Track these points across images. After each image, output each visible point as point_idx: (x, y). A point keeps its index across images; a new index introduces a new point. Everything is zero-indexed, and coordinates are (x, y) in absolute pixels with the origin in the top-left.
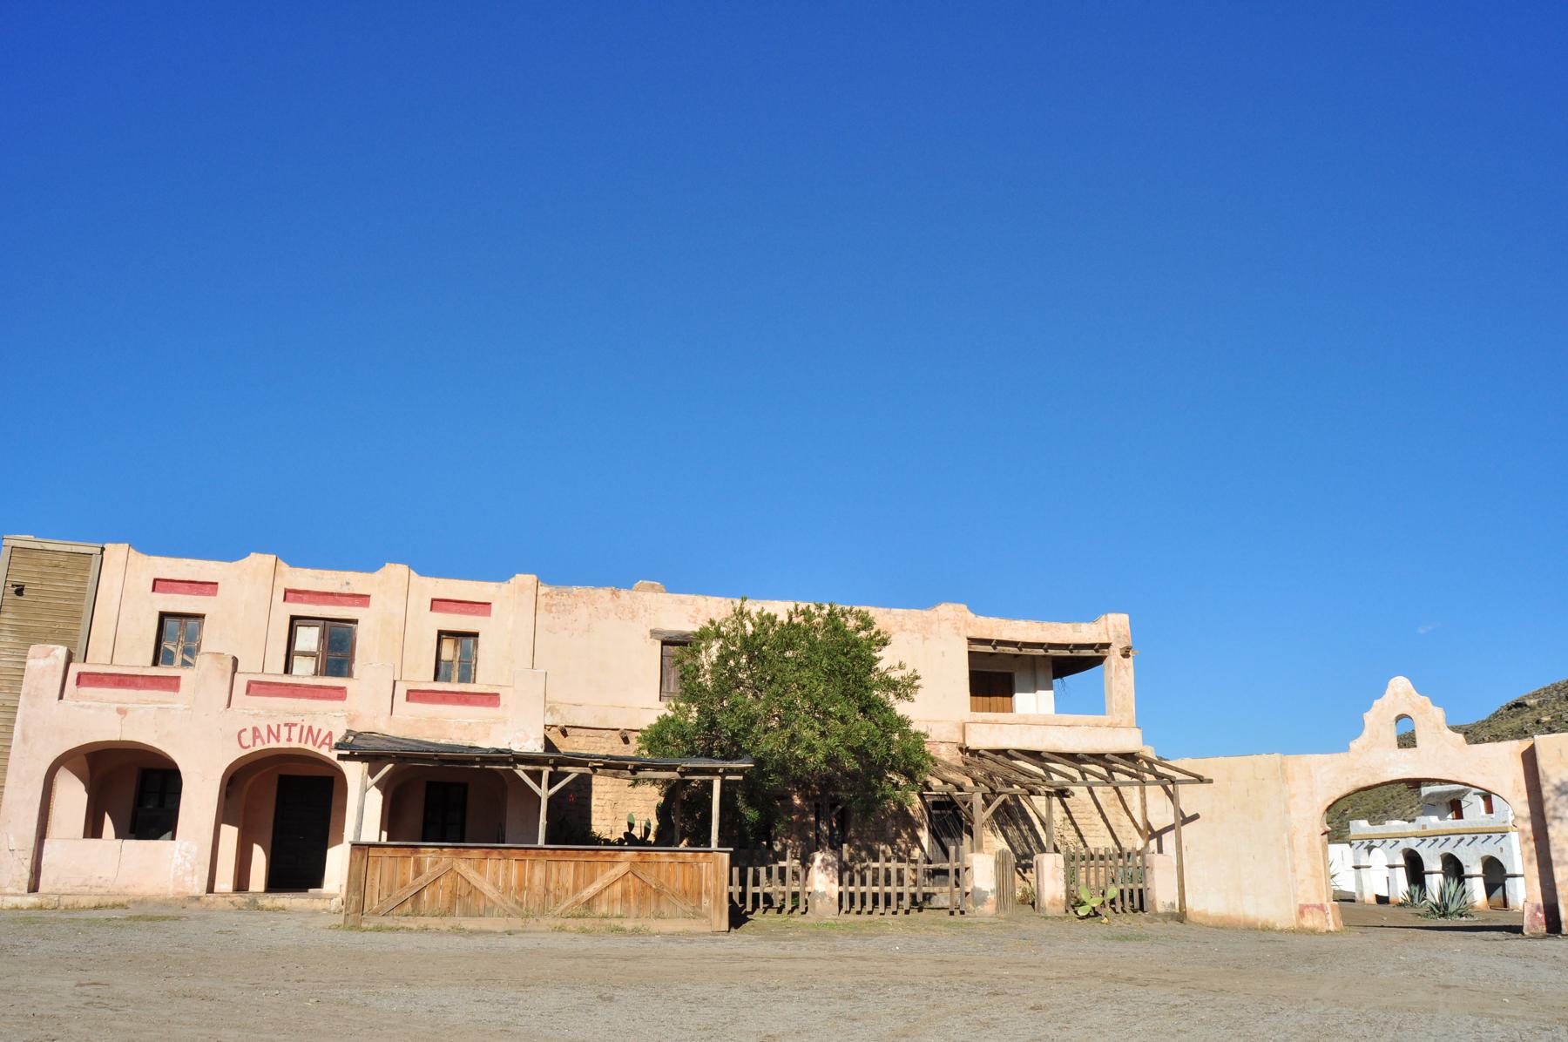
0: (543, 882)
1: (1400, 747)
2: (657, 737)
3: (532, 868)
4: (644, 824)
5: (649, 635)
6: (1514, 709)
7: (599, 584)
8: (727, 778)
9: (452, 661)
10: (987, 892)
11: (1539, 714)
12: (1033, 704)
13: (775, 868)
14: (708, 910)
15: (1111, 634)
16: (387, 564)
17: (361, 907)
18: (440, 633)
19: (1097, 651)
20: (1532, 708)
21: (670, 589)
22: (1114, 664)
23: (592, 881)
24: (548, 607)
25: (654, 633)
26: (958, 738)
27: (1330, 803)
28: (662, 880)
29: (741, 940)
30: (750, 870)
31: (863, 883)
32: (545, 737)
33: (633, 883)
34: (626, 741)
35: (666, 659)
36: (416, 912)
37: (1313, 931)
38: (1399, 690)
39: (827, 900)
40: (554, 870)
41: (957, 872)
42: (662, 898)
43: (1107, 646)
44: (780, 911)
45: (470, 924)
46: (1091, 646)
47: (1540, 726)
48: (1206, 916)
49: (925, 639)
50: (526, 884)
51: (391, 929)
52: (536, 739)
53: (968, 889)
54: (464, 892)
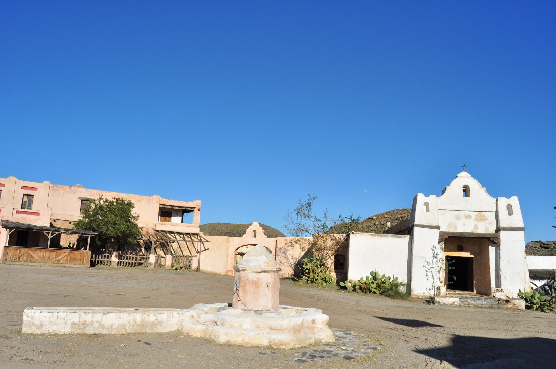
0: (48, 256)
1: (256, 237)
2: (78, 224)
3: (46, 253)
4: (73, 243)
5: (78, 198)
6: (369, 219)
7: (66, 185)
8: (92, 236)
9: (26, 202)
10: (152, 263)
11: (375, 221)
12: (176, 220)
13: (103, 255)
14: (85, 263)
15: (196, 205)
16: (10, 177)
17: (6, 260)
18: (24, 194)
19: (192, 209)
20: (374, 220)
21: (84, 187)
22: (195, 212)
23: (59, 256)
24: (53, 190)
25: (80, 198)
26: (154, 227)
27: (237, 248)
28: (76, 257)
29: (93, 270)
30: (97, 255)
31: (124, 259)
32: (50, 222)
33: (69, 257)
34: (70, 223)
35: (82, 204)
36: (19, 261)
37: (229, 276)
38: (255, 225)
39: (115, 263)
40: (51, 254)
41: (146, 258)
42: (75, 260)
43: (195, 208)
44: (104, 265)
45: (31, 264)
46: (190, 208)
47: (375, 225)
48: (207, 271)
49: (149, 203)
50: (45, 256)
51: (13, 264)
52: (48, 224)
53: (149, 262)
54: (30, 257)
